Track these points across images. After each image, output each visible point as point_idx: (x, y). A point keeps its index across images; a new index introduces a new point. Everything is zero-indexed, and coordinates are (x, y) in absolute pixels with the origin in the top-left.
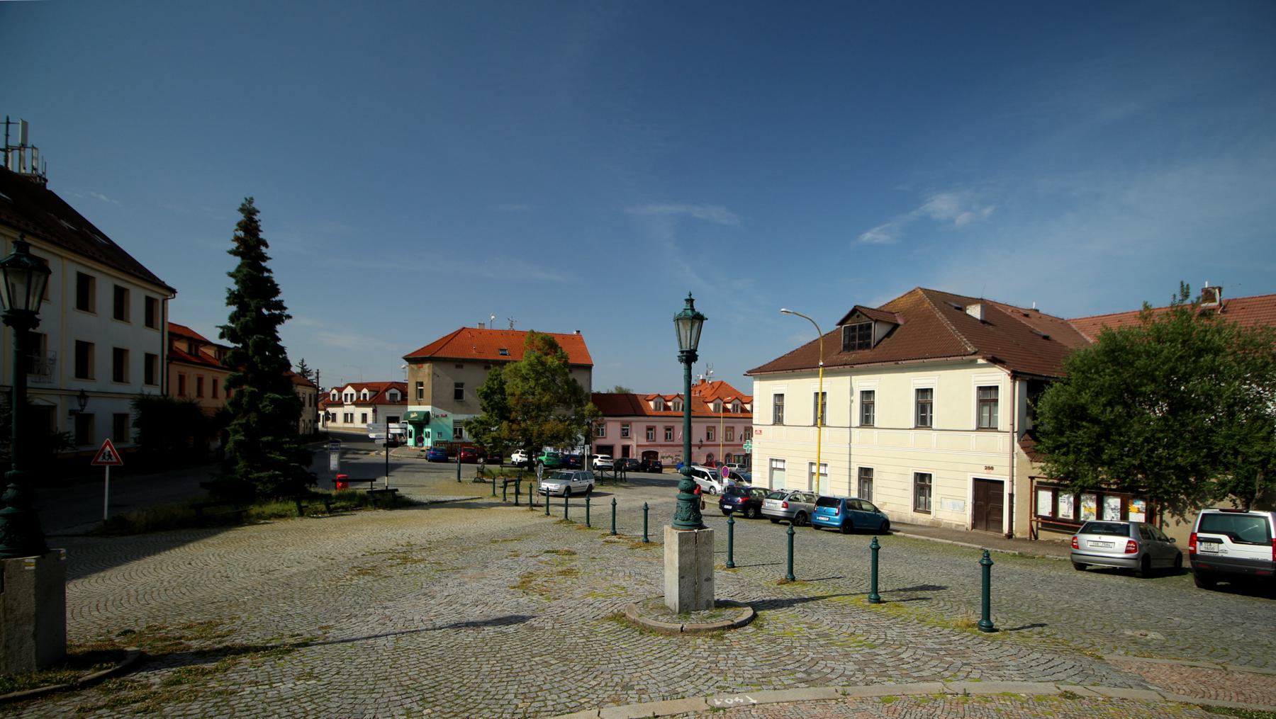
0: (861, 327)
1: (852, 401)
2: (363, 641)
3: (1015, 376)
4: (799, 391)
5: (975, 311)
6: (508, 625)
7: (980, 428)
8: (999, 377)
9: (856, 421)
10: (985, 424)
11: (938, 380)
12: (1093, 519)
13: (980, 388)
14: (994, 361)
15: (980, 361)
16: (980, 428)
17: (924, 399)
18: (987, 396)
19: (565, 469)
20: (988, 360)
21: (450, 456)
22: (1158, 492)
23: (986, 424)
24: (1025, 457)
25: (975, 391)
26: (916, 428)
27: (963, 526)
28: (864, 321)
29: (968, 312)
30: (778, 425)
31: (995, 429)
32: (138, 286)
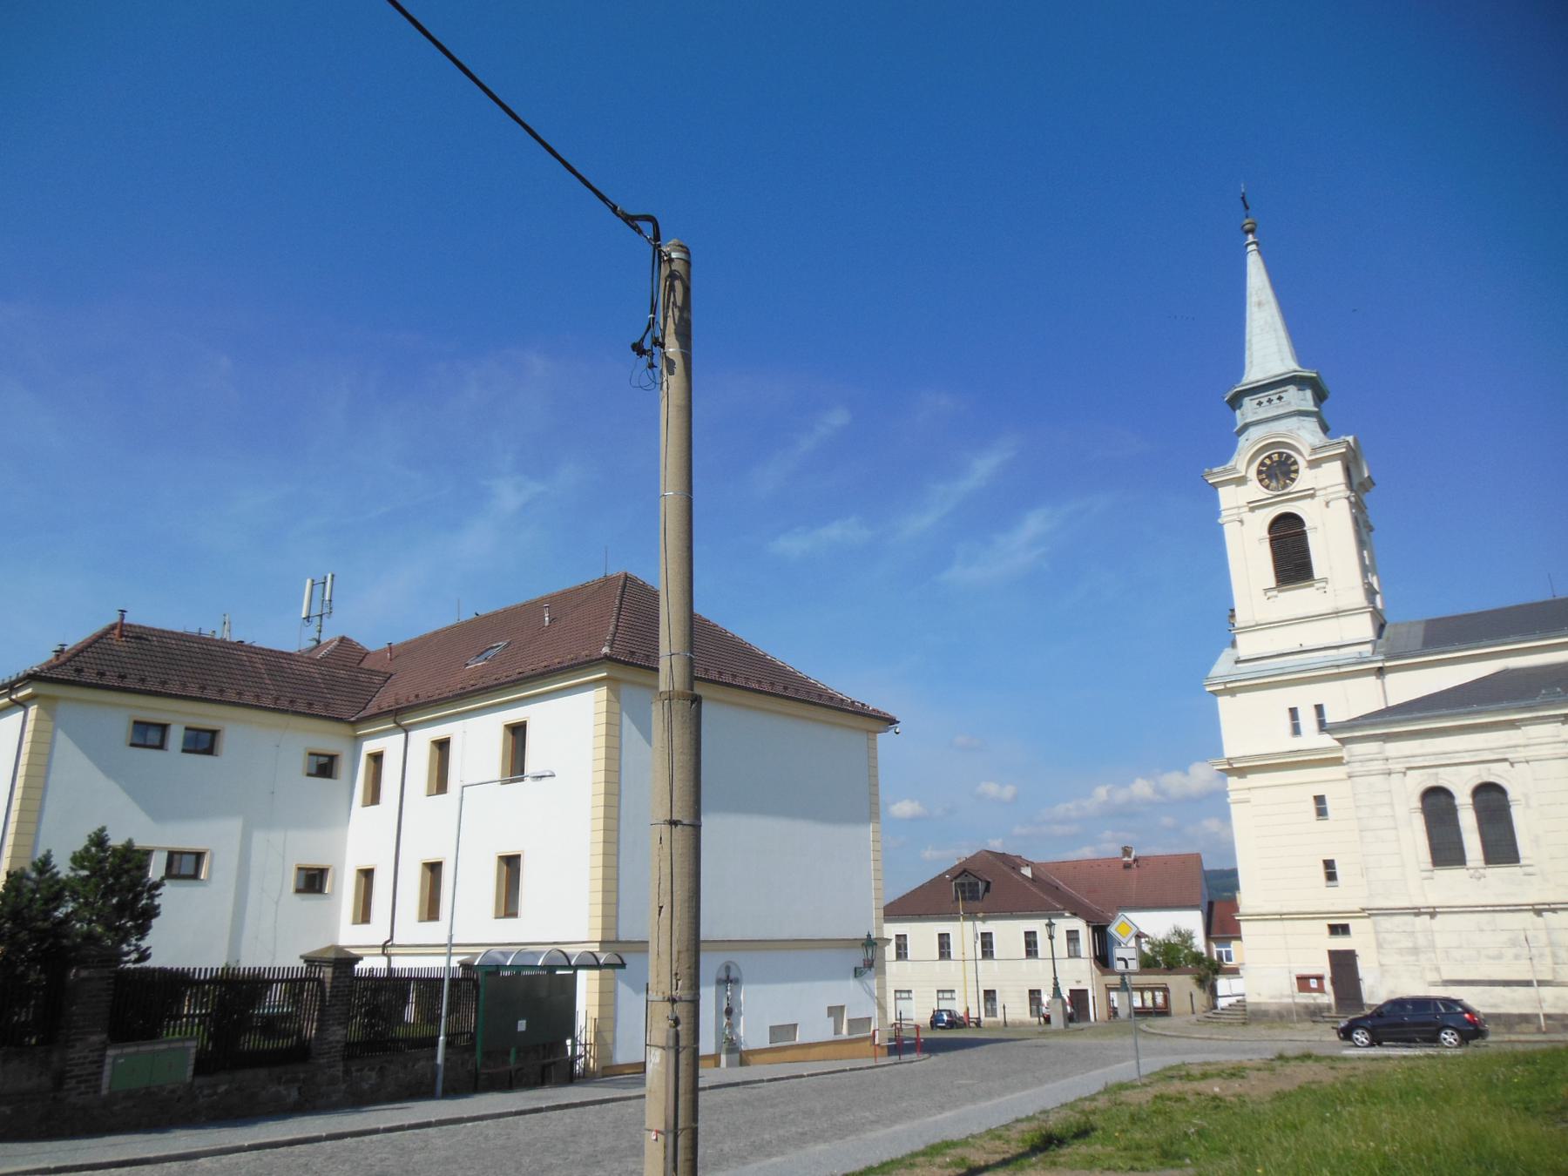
0: (970, 884)
1: (975, 942)
2: (1235, 1038)
3: (1088, 923)
4: (921, 935)
5: (1027, 872)
6: (1450, 1003)
7: (1070, 957)
8: (1079, 925)
9: (980, 955)
10: (1072, 954)
11: (999, 928)
12: (1157, 993)
13: (1068, 932)
14: (1075, 915)
15: (1067, 914)
16: (1070, 957)
17: (944, 940)
18: (1072, 936)
19: (317, 1026)
20: (1072, 914)
21: (874, 994)
22: (185, 1012)
23: (1074, 954)
24: (1098, 972)
25: (1065, 933)
26: (897, 960)
27: (668, 1031)
28: (972, 879)
29: (1022, 872)
30: (945, 959)
31: (1080, 957)
32: (1258, 915)
